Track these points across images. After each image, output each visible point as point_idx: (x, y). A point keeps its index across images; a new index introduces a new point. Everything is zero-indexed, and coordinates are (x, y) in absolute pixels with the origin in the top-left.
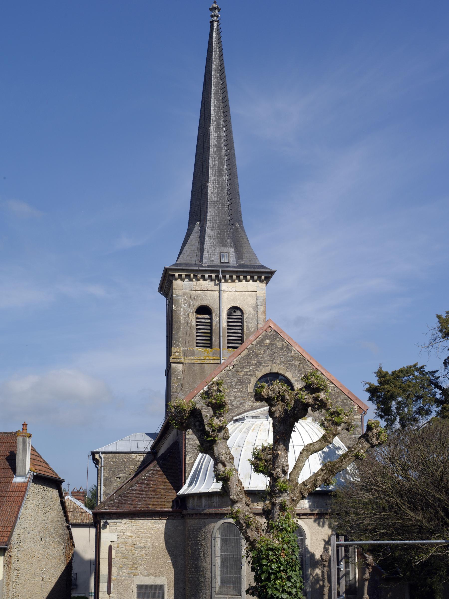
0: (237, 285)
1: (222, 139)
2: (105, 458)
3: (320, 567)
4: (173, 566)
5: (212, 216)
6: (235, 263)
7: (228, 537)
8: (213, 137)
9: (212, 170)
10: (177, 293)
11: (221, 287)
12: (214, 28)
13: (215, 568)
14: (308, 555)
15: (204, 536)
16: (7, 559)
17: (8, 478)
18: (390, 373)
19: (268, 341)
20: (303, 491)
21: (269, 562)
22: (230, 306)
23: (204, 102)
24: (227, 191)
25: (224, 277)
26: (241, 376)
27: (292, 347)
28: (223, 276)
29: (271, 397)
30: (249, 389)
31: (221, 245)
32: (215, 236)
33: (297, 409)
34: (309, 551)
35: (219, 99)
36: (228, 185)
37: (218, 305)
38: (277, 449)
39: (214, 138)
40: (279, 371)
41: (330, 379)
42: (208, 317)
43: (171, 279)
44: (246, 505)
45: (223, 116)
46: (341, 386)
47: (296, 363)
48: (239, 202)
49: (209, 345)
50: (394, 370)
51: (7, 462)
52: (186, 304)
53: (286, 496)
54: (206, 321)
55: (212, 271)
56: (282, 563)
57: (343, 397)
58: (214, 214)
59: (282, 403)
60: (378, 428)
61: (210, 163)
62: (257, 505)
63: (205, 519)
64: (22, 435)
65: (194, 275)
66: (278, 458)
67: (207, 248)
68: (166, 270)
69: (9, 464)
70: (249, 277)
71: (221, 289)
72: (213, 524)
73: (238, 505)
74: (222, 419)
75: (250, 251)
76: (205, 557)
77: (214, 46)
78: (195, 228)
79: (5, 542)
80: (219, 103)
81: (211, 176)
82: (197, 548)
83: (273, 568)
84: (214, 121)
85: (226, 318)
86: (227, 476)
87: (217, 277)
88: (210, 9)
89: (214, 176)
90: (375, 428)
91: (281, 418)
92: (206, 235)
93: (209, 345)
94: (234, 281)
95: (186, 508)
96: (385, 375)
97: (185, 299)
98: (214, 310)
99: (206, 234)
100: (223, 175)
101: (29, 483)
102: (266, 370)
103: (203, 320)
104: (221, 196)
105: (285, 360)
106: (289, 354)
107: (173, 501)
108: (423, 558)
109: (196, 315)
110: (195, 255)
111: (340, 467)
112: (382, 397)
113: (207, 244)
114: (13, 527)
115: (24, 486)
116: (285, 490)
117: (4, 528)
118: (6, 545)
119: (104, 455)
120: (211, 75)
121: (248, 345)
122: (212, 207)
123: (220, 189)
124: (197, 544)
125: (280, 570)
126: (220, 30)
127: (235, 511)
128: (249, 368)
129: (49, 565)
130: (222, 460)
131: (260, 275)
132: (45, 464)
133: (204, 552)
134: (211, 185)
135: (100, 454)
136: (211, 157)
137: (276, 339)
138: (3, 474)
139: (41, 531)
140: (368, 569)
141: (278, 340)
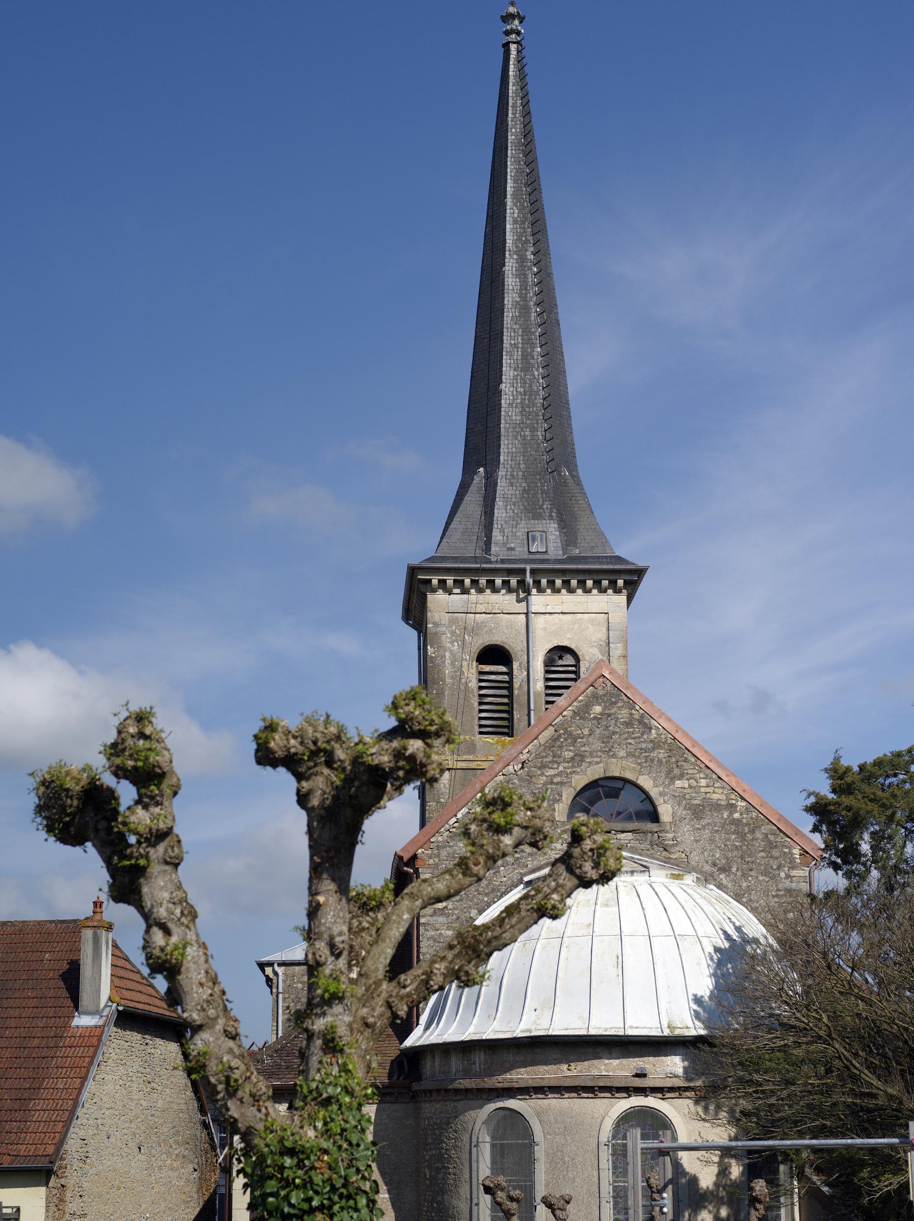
0: (565, 601)
1: (531, 291)
2: (285, 974)
3: (711, 1208)
4: (392, 1206)
5: (510, 455)
6: (561, 552)
7: (505, 1142)
8: (511, 287)
9: (508, 357)
10: (437, 619)
11: (530, 605)
12: (511, 56)
13: (478, 1209)
14: (684, 1180)
15: (456, 1139)
16: (54, 1192)
17: (62, 1019)
18: (856, 769)
19: (598, 709)
20: (393, 1002)
21: (283, 1188)
22: (550, 646)
23: (491, 214)
24: (542, 401)
25: (537, 583)
26: (540, 786)
27: (652, 721)
28: (534, 582)
29: (295, 754)
30: (556, 814)
31: (531, 515)
32: (517, 496)
33: (356, 783)
34: (684, 1170)
35: (523, 205)
36: (543, 388)
37: (525, 645)
38: (316, 889)
39: (513, 289)
40: (622, 772)
41: (736, 789)
42: (503, 669)
43: (423, 590)
44: (227, 1036)
45: (532, 242)
46: (761, 805)
47: (661, 756)
48: (570, 425)
49: (506, 730)
50: (862, 762)
51: (62, 984)
52: (456, 644)
53: (340, 1014)
54: (500, 678)
55: (510, 572)
56: (315, 1187)
57: (766, 828)
58: (514, 450)
59: (326, 771)
60: (596, 837)
61: (505, 341)
62: (569, 1070)
63: (456, 1101)
64: (91, 924)
65: (472, 581)
66: (319, 913)
67: (499, 522)
68: (413, 571)
69: (67, 989)
70: (590, 583)
71: (530, 609)
72: (473, 1113)
73: (205, 1035)
74: (157, 810)
75: (593, 527)
76: (456, 1187)
77: (510, 94)
78: (474, 482)
79: (49, 1155)
80: (523, 214)
81: (508, 369)
82: (440, 1165)
83: (293, 1201)
84: (512, 253)
85: (543, 671)
86: (171, 959)
87: (521, 583)
88: (502, 17)
89: (515, 370)
90: (589, 837)
91: (325, 808)
92: (497, 495)
93: (506, 728)
94: (559, 591)
95: (419, 1078)
96: (845, 773)
97: (453, 633)
98: (516, 654)
99: (498, 492)
100: (533, 366)
101: (106, 1028)
102: (594, 772)
103: (493, 677)
104: (530, 412)
105: (636, 749)
106: (645, 737)
107: (392, 1066)
108: (890, 1184)
109: (477, 666)
110: (475, 537)
111: (496, 938)
112: (839, 825)
113: (500, 515)
114: (68, 1124)
115: (96, 1034)
116: (341, 999)
117: (49, 1125)
118: (51, 1162)
119: (283, 968)
120: (507, 157)
121: (554, 716)
122: (510, 434)
123: (527, 397)
124: (440, 1157)
125: (311, 1206)
126: (524, 61)
127: (195, 1053)
128: (557, 768)
129: (161, 1204)
130: (160, 919)
131: (613, 577)
132: (149, 988)
133: (455, 1174)
134: (507, 389)
135: (276, 966)
136: (507, 328)
137: (615, 703)
138: (54, 1009)
139: (138, 1131)
140: (756, 1210)
141: (620, 704)
